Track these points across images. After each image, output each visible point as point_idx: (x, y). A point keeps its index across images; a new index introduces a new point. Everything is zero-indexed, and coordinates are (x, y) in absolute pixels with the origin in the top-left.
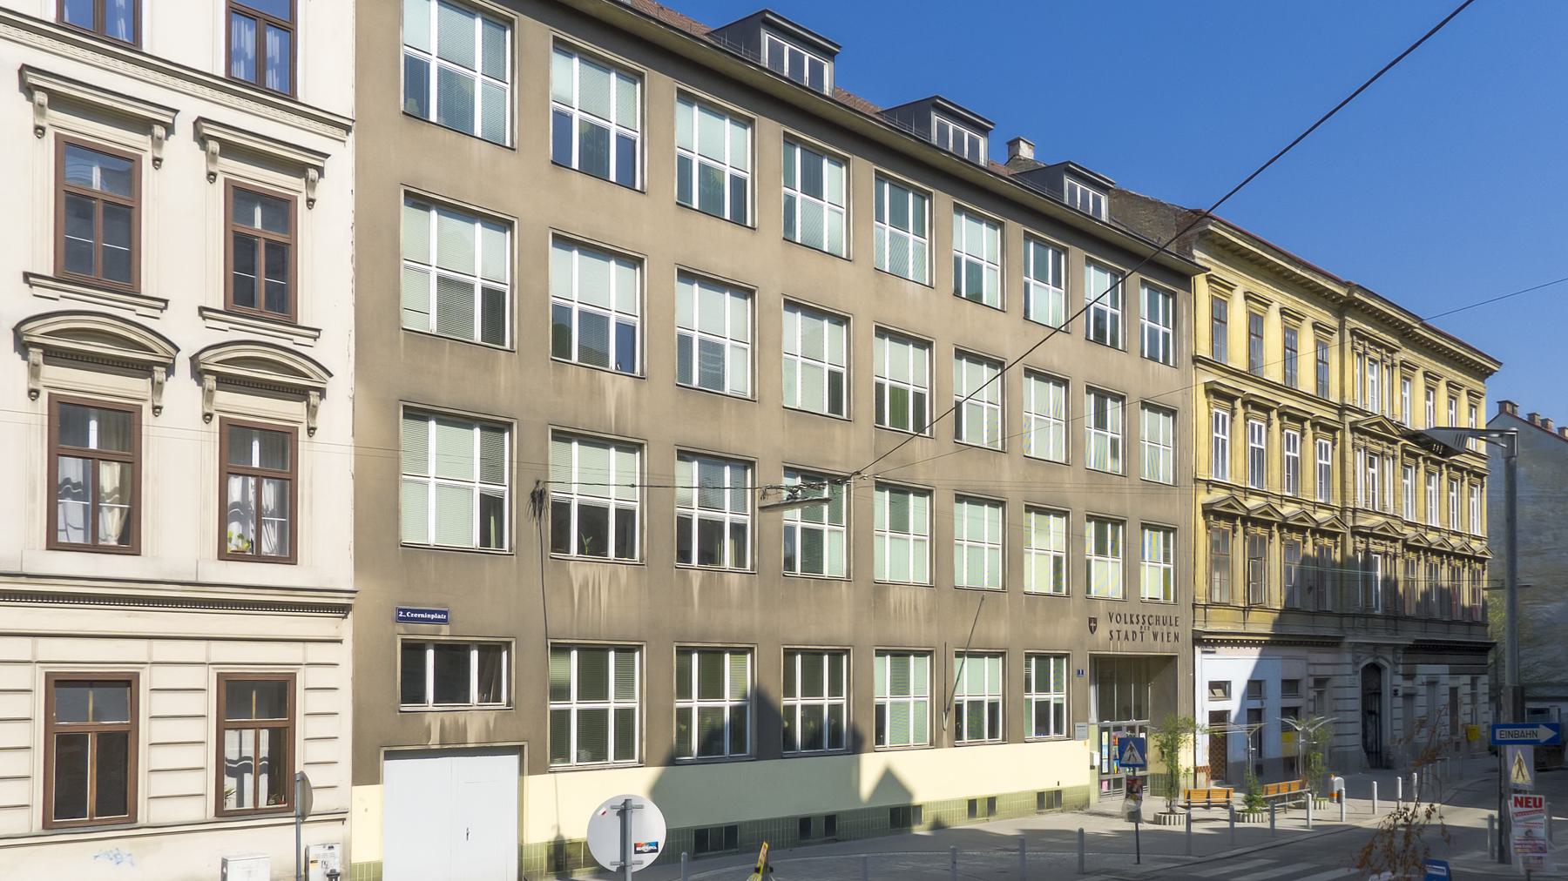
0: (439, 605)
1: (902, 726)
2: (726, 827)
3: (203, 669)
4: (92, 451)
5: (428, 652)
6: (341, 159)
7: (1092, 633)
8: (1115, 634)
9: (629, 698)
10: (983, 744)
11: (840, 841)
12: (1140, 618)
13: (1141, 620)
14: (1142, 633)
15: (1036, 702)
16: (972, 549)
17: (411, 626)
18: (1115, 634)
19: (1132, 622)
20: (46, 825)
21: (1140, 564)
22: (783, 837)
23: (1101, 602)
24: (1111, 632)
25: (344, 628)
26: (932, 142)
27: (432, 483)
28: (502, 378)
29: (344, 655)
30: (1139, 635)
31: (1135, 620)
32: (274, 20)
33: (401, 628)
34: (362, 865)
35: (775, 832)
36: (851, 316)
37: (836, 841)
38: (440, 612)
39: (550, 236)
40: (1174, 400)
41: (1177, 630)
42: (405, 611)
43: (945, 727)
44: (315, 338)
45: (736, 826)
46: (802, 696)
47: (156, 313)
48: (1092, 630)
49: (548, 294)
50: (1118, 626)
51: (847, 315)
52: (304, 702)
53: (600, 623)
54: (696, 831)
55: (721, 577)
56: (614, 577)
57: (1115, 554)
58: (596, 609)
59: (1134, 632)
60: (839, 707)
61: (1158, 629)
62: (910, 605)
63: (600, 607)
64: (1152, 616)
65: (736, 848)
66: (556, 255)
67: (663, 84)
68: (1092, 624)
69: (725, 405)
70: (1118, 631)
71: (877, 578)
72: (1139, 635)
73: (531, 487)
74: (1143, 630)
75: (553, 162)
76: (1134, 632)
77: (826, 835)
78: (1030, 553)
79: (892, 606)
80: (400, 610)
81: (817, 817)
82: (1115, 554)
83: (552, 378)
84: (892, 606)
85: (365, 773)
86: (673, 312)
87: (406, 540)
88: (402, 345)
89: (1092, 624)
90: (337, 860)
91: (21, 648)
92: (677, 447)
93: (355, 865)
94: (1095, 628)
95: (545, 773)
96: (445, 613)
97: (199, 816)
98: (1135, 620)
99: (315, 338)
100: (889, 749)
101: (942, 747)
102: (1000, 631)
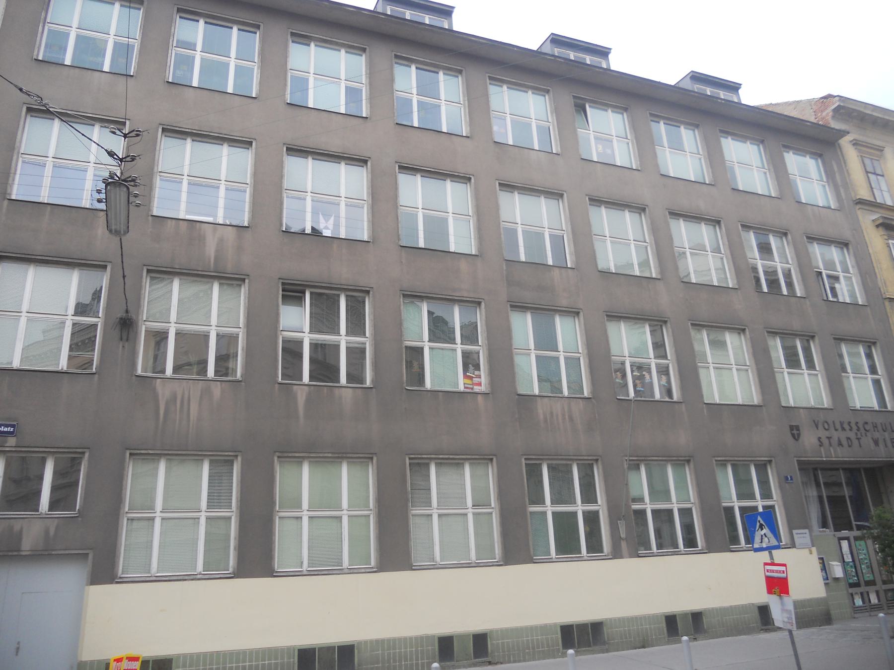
5: (751, 466)
7: (797, 440)
8: (826, 442)
9: (298, 508)
10: (581, 559)
11: (496, 664)
12: (853, 425)
13: (854, 427)
14: (858, 439)
18: (826, 442)
19: (843, 429)
21: (841, 376)
22: (417, 659)
24: (819, 439)
26: (388, 13)
27: (711, 366)
30: (856, 442)
31: (846, 426)
35: (411, 652)
37: (490, 663)
39: (498, 184)
40: (847, 235)
43: (623, 535)
45: (353, 646)
46: (582, 503)
48: (796, 437)
49: (499, 220)
50: (827, 434)
51: (561, 192)
54: (299, 650)
56: (206, 393)
57: (811, 365)
59: (848, 439)
60: (596, 514)
61: (877, 435)
62: (564, 415)
64: (866, 423)
66: (404, 180)
67: (383, 52)
68: (795, 432)
70: (828, 438)
71: (521, 391)
72: (856, 442)
73: (120, 314)
74: (859, 436)
76: (848, 439)
77: (475, 657)
78: (848, 377)
79: (542, 417)
81: (463, 637)
82: (811, 365)
84: (542, 417)
86: (281, 177)
89: (795, 432)
92: (281, 281)
94: (799, 435)
95: (112, 583)
98: (846, 426)
100: (586, 558)
102: (682, 439)
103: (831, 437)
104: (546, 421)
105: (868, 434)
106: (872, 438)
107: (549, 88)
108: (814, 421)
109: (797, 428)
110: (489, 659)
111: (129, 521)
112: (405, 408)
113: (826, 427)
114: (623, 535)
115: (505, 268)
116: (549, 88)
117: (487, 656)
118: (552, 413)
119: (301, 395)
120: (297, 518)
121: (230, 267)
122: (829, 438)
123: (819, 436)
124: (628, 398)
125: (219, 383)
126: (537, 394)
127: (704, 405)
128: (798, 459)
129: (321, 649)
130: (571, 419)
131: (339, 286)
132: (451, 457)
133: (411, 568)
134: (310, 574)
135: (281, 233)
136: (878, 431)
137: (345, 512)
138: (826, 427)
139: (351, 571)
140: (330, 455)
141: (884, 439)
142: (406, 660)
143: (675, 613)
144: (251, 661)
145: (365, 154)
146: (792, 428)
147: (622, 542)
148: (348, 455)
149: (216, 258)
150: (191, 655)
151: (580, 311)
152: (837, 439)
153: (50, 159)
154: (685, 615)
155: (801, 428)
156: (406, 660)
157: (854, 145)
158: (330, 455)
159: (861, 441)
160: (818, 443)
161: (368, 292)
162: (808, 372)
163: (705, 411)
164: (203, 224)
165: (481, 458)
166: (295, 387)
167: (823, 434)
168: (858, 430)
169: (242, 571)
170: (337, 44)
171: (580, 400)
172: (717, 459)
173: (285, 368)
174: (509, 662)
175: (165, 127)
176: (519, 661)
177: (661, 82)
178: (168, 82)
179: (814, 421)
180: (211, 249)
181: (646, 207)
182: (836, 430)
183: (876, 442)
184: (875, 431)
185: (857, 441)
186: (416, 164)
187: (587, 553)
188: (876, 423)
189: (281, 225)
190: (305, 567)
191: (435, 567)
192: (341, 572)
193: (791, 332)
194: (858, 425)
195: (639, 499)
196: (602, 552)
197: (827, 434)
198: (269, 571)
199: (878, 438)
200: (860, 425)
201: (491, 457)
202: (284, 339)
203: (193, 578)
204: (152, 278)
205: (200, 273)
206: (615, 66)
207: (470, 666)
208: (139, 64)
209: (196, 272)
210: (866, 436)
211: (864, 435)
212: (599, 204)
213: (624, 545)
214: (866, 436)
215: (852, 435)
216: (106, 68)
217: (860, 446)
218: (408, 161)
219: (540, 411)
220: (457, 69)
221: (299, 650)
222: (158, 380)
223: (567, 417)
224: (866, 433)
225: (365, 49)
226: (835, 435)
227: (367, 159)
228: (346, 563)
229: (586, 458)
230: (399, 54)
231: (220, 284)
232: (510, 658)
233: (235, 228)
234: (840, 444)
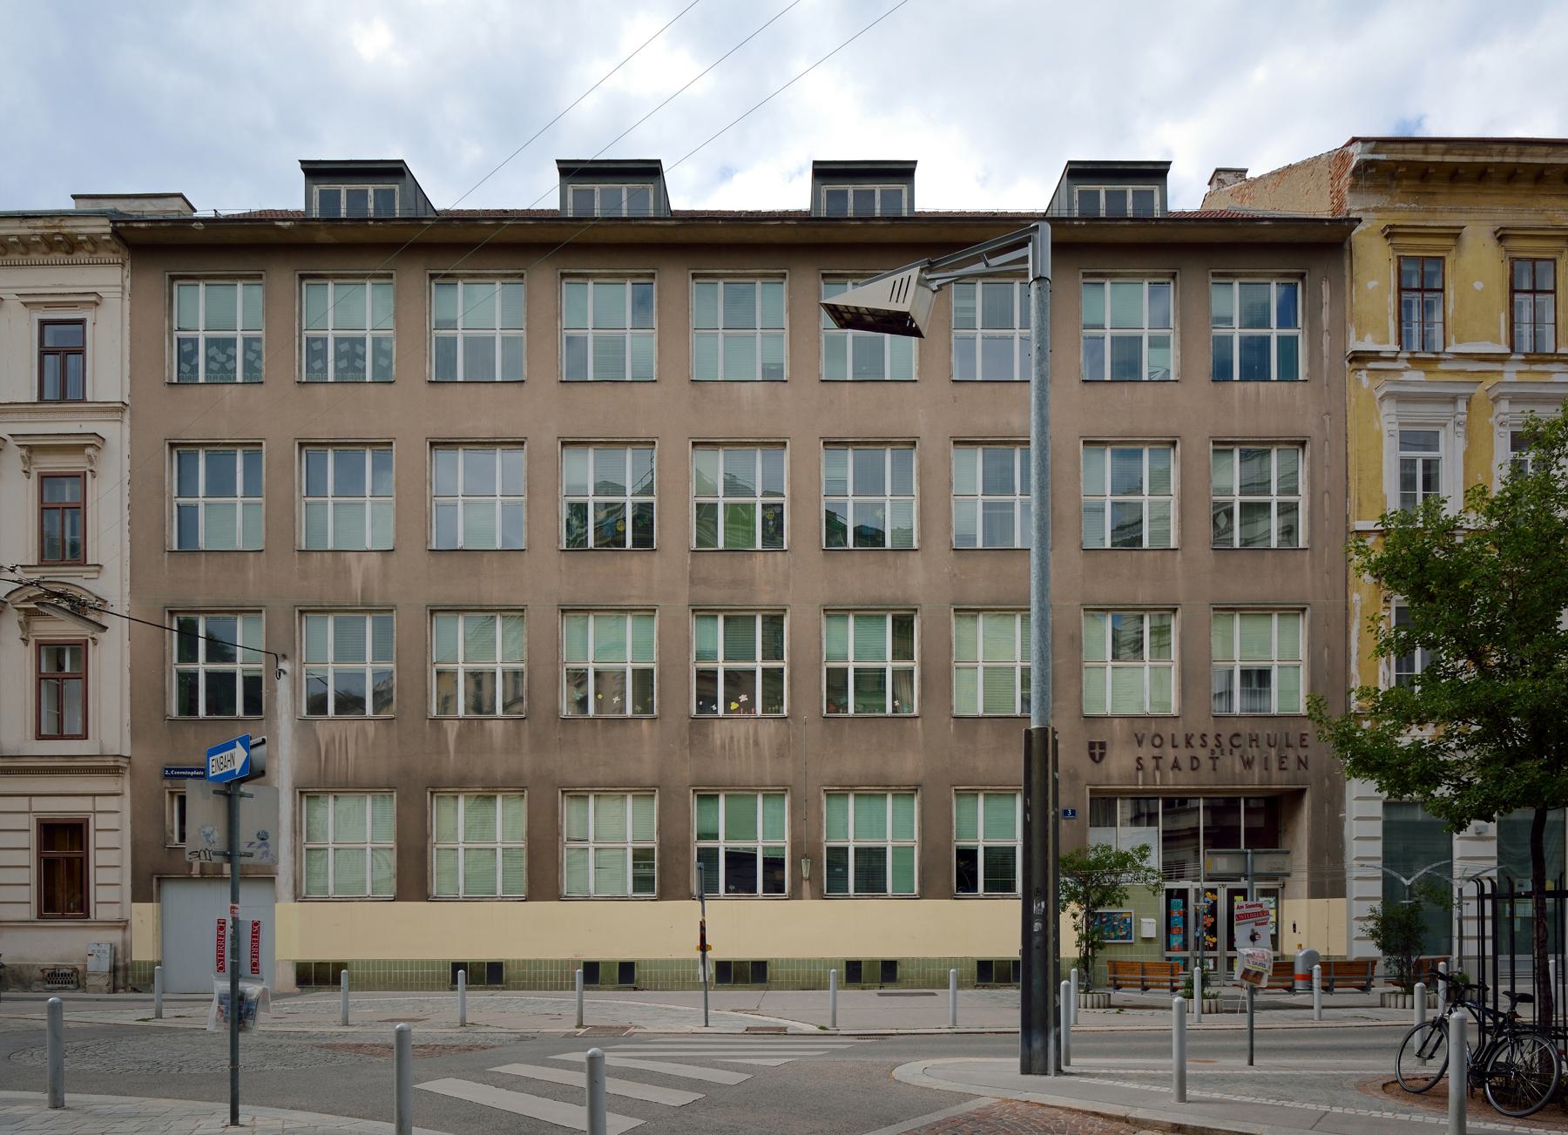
0: (198, 764)
1: (903, 871)
2: (488, 963)
3: (26, 816)
4: (67, 673)
6: (116, 433)
8: (1149, 764)
15: (727, 853)
16: (1118, 670)
17: (175, 782)
20: (40, 916)
23: (1117, 721)
25: (124, 784)
28: (251, 575)
29: (125, 805)
32: (71, 349)
33: (167, 783)
34: (139, 962)
36: (786, 440)
37: (635, 989)
38: (198, 770)
41: (1302, 753)
42: (170, 770)
44: (98, 572)
47: (95, 575)
52: (96, 840)
53: (347, 773)
54: (453, 963)
55: (482, 725)
58: (344, 762)
62: (747, 739)
63: (347, 759)
65: (502, 983)
69: (485, 560)
75: (1213, 381)
77: (620, 983)
79: (718, 742)
80: (166, 769)
81: (608, 964)
83: (297, 566)
84: (718, 742)
85: (142, 892)
87: (1086, 713)
88: (166, 564)
90: (108, 955)
91: (22, 804)
93: (135, 961)
94: (1102, 755)
96: (203, 770)
97: (26, 916)
99: (98, 572)
100: (982, 896)
101: (801, 898)
103: (1161, 758)
104: (723, 747)
105: (1237, 752)
106: (1242, 757)
107: (784, 271)
108: (1136, 735)
109: (1103, 745)
110: (634, 985)
111: (467, 852)
112: (560, 739)
113: (1157, 742)
114: (805, 874)
115: (689, 562)
116: (784, 271)
117: (632, 982)
118: (732, 738)
119: (452, 729)
120: (454, 849)
121: (377, 601)
122: (1157, 758)
123: (1140, 755)
124: (883, 714)
125: (372, 722)
126: (1019, 715)
127: (952, 720)
128: (1092, 787)
129: (736, 962)
130: (756, 743)
131: (490, 608)
132: (607, 789)
133: (558, 897)
134: (466, 900)
135: (428, 552)
136: (1257, 746)
137: (499, 845)
138: (1157, 742)
139: (503, 899)
140: (480, 789)
141: (1266, 758)
142: (551, 979)
143: (860, 959)
144: (385, 969)
145: (518, 434)
146: (1092, 745)
147: (804, 882)
148: (499, 789)
149: (363, 591)
150: (363, 961)
151: (1178, 606)
152: (1172, 759)
153: (499, 498)
154: (872, 963)
155: (1108, 747)
156: (551, 979)
157: (1387, 237)
158: (480, 789)
159: (1218, 762)
160: (1136, 765)
161: (916, 610)
162: (1113, 663)
163: (952, 726)
164: (348, 554)
165: (643, 791)
166: (445, 722)
167: (1146, 752)
168: (1219, 745)
169: (401, 896)
170: (488, 276)
171: (771, 720)
172: (957, 788)
173: (769, 698)
174: (656, 990)
175: (300, 441)
176: (668, 990)
177: (223, 213)
178: (561, 381)
179: (1136, 735)
180: (357, 584)
181: (916, 440)
182: (1174, 746)
183: (1248, 764)
184: (1251, 746)
185: (1211, 762)
186: (887, 436)
187: (985, 891)
188: (1257, 735)
189: (294, 545)
190: (461, 894)
191: (587, 899)
192: (493, 899)
193: (478, 608)
194: (1221, 739)
195: (712, 834)
196: (784, 892)
197: (1156, 752)
198: (424, 896)
199: (1253, 757)
200: (1225, 741)
201: (653, 789)
202: (337, 672)
203: (361, 900)
204: (828, 616)
205: (348, 608)
206: (680, 201)
207: (614, 990)
208: (659, 369)
209: (344, 608)
210: (1231, 754)
211: (1227, 752)
212: (845, 448)
213: (806, 886)
214: (1231, 754)
215: (1203, 754)
216: (1108, 377)
217: (1214, 769)
218: (572, 433)
219: (717, 736)
220: (1278, 273)
221: (453, 963)
222: (318, 722)
223: (751, 741)
224: (1231, 750)
225: (785, 274)
226: (1170, 754)
227: (523, 440)
228: (499, 892)
229: (769, 788)
230: (566, 271)
231: (984, 615)
232: (657, 986)
233: (379, 553)
234: (1176, 766)
